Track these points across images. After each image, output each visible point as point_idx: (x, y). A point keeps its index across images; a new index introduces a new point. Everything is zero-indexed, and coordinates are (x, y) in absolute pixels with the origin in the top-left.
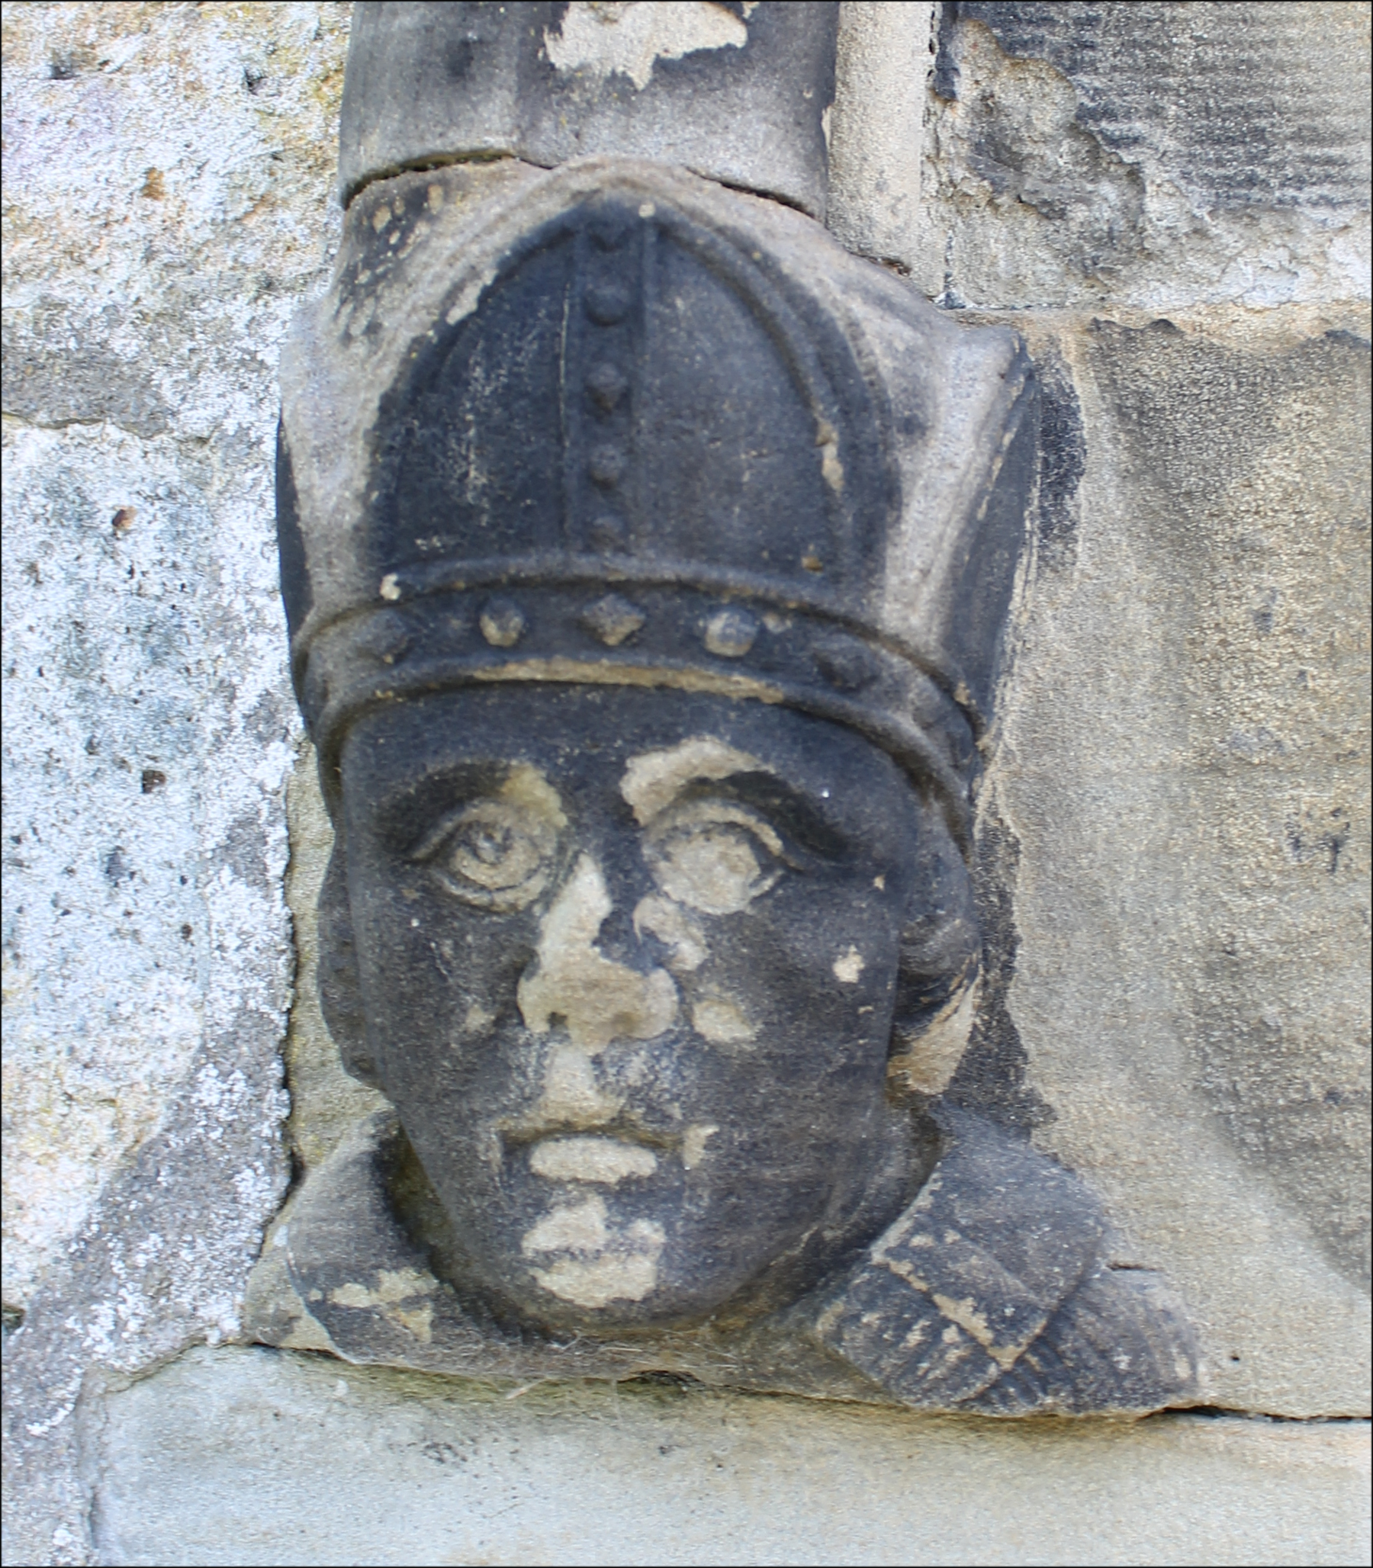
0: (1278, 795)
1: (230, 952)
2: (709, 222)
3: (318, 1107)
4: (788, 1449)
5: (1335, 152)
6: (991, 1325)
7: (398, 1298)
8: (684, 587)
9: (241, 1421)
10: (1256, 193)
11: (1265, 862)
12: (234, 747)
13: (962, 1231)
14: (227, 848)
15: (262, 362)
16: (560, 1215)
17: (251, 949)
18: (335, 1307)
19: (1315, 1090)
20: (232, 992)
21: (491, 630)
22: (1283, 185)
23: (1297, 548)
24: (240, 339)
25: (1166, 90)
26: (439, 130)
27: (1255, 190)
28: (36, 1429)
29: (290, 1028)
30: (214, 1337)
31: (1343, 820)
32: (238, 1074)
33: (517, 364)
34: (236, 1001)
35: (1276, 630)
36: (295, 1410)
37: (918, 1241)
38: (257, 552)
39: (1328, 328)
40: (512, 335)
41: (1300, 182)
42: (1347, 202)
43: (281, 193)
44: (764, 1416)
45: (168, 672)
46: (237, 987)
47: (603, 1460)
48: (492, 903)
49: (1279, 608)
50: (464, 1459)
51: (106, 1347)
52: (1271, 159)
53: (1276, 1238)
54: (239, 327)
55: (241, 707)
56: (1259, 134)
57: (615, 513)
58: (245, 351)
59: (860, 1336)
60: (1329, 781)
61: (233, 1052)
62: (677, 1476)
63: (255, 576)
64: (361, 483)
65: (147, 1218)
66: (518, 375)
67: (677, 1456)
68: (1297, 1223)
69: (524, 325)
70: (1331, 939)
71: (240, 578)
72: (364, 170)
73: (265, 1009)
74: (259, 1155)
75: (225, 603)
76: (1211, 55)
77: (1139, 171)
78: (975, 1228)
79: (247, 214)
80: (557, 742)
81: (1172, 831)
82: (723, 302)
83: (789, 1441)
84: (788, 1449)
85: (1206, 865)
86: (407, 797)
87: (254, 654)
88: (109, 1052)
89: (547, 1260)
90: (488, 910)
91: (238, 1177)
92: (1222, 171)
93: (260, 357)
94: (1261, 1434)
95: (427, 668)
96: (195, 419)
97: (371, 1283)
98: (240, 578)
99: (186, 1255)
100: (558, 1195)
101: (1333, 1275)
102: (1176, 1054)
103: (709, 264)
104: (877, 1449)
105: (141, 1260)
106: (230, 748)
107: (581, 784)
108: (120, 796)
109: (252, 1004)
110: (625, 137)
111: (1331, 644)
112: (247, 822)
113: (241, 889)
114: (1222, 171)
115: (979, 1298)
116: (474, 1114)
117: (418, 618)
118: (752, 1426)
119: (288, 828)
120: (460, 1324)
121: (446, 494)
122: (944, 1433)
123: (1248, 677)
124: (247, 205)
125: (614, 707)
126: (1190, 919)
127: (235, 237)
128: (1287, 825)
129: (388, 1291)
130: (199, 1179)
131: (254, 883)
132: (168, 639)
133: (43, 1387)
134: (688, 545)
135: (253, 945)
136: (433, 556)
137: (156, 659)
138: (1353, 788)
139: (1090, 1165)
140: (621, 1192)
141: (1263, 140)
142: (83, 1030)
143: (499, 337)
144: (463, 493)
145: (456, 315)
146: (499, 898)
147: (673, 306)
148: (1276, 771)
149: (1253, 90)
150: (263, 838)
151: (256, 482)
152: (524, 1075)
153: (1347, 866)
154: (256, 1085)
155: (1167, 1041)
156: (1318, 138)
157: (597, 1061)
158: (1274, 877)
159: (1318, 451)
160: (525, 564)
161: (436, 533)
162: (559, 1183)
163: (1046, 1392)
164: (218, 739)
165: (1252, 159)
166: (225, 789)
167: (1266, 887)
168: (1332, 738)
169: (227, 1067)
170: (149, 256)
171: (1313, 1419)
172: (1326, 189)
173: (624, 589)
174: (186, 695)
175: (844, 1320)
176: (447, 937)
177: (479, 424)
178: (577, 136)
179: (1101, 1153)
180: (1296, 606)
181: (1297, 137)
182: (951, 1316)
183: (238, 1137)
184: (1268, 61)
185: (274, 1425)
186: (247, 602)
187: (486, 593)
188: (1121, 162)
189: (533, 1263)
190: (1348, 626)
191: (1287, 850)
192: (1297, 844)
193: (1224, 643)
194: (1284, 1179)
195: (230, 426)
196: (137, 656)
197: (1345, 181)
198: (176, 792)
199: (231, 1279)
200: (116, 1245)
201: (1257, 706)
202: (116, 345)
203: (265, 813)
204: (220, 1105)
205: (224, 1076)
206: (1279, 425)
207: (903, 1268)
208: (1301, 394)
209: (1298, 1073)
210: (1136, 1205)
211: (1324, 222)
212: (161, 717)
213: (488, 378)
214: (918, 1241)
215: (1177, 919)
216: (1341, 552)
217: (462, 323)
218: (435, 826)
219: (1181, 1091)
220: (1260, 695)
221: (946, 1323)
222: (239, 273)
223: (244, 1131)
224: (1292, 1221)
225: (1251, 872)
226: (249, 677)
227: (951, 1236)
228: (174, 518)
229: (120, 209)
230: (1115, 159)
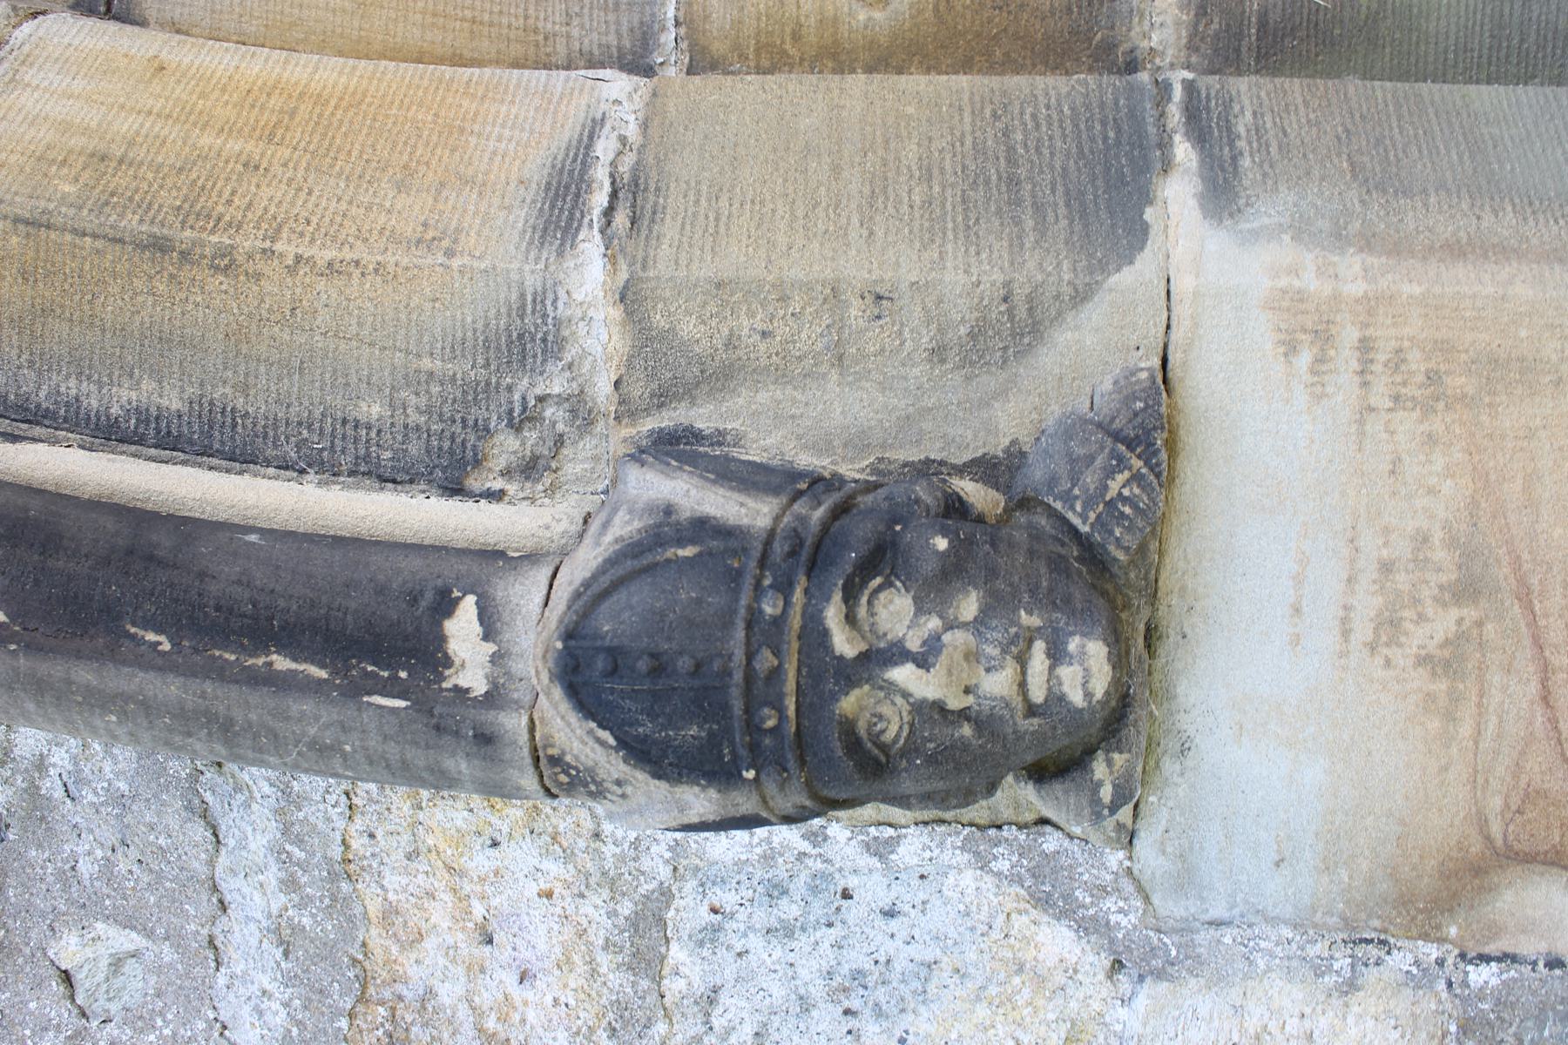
2: (565, 613)
3: (1011, 811)
5: (529, 298)
6: (1121, 472)
8: (749, 626)
9: (1169, 850)
10: (550, 338)
13: (1073, 486)
19: (1003, 308)
25: (498, 383)
28: (1174, 953)
29: (971, 825)
30: (1127, 863)
34: (958, 852)
37: (1078, 509)
41: (545, 316)
45: (792, 886)
49: (760, 326)
51: (1132, 917)
53: (1077, 328)
54: (618, 850)
56: (521, 336)
65: (1068, 897)
67: (1187, 630)
76: (480, 361)
82: (605, 607)
88: (983, 916)
89: (1088, 695)
90: (912, 725)
94: (1175, 335)
96: (664, 872)
97: (1100, 784)
99: (1086, 877)
100: (1056, 689)
102: (984, 378)
105: (1088, 900)
106: (830, 855)
107: (848, 678)
108: (854, 911)
112: (867, 846)
113: (901, 850)
115: (1107, 477)
116: (1015, 732)
123: (794, 342)
124: (556, 847)
126: (916, 371)
130: (1047, 870)
132: (775, 886)
133: (1152, 949)
137: (785, 892)
142: (972, 929)
145: (612, 741)
146: (906, 719)
150: (876, 838)
151: (696, 842)
157: (988, 670)
160: (737, 706)
162: (1049, 689)
167: (900, 333)
170: (582, 896)
172: (548, 303)
173: (750, 656)
174: (804, 877)
181: (522, 318)
187: (752, 726)
192: (879, 317)
194: (1047, 323)
195: (668, 855)
196: (784, 902)
198: (852, 882)
200: (1080, 913)
202: (627, 912)
205: (995, 858)
207: (1092, 516)
212: (814, 890)
214: (1078, 509)
217: (616, 738)
218: (869, 752)
220: (804, 336)
221: (1120, 494)
227: (1076, 491)
228: (714, 883)
229: (558, 910)
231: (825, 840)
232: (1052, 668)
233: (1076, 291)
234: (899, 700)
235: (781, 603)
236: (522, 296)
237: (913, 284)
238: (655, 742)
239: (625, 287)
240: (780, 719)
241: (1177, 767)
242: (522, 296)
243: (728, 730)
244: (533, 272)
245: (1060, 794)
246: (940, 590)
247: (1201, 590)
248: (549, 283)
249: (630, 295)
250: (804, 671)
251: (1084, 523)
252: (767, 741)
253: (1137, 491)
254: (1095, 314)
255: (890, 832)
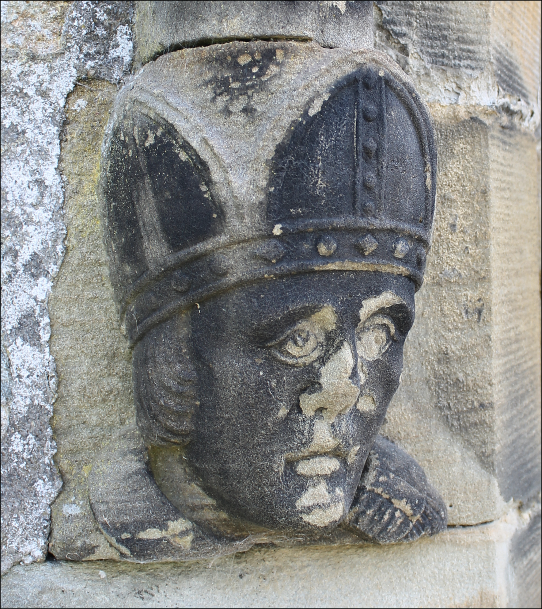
0: (460, 294)
1: (24, 378)
2: (401, 80)
3: (69, 447)
4: (291, 567)
5: (471, 48)
6: (412, 508)
7: (178, 532)
8: (391, 231)
10: (446, 61)
11: (456, 319)
12: (19, 280)
13: (394, 472)
14: (19, 328)
15: (26, 93)
16: (311, 490)
17: (35, 376)
18: (140, 540)
19: (476, 404)
20: (26, 397)
21: (323, 249)
22: (454, 59)
23: (463, 200)
24: (15, 81)
25: (412, 15)
26: (282, 24)
27: (445, 59)
29: (55, 411)
31: (482, 302)
32: (30, 436)
33: (338, 136)
34: (28, 401)
35: (457, 231)
36: (70, 587)
37: (381, 479)
38: (25, 185)
39: (470, 115)
40: (336, 123)
41: (460, 59)
42: (477, 68)
43: (31, 11)
44: (280, 556)
46: (28, 394)
47: (215, 586)
48: (297, 363)
50: (153, 596)
52: (450, 48)
53: (464, 460)
55: (21, 261)
56: (445, 37)
57: (373, 201)
58: (17, 88)
59: (365, 520)
60: (476, 288)
61: (28, 425)
62: (246, 586)
63: (25, 197)
64: (264, 183)
66: (339, 141)
67: (245, 579)
68: (471, 453)
69: (341, 119)
70: (479, 347)
71: (17, 198)
72: (233, 33)
73: (42, 404)
74: (45, 472)
75: (10, 209)
77: (406, 47)
78: (397, 471)
79: (15, 20)
80: (338, 295)
81: (424, 309)
82: (404, 113)
83: (291, 564)
84: (291, 567)
85: (436, 321)
86: (277, 321)
87: (28, 235)
89: (309, 510)
90: (293, 366)
91: (36, 484)
92: (433, 51)
93: (25, 91)
95: (294, 265)
97: (163, 526)
98: (17, 198)
99: (15, 524)
100: (310, 482)
101: (483, 471)
102: (428, 394)
103: (399, 96)
104: (326, 561)
106: (17, 280)
109: (36, 402)
110: (339, 34)
111: (476, 237)
112: (29, 315)
113: (27, 348)
114: (433, 51)
115: (407, 498)
117: (288, 243)
118: (276, 560)
119: (50, 318)
120: (204, 539)
121: (307, 190)
122: (350, 551)
123: (448, 249)
124: (15, 16)
125: (359, 280)
126: (431, 342)
127: (10, 30)
128: (464, 305)
129: (173, 530)
130: (17, 487)
131: (35, 345)
134: (395, 214)
135: (36, 374)
136: (298, 216)
138: (484, 290)
139: (399, 439)
140: (332, 477)
141: (446, 40)
143: (331, 124)
144: (314, 190)
145: (312, 112)
146: (300, 361)
147: (390, 114)
148: (459, 284)
149: (442, 19)
150: (38, 323)
151: (23, 152)
152: (303, 434)
153: (483, 320)
154: (40, 440)
155: (425, 389)
156: (464, 42)
157: (333, 425)
158: (460, 325)
159: (469, 163)
160: (339, 222)
161: (301, 207)
162: (311, 477)
163: (423, 530)
164: (10, 276)
165: (443, 47)
166: (15, 301)
167: (456, 328)
168: (477, 272)
169: (25, 432)
171: (477, 525)
172: (469, 62)
173: (372, 232)
175: (358, 514)
176: (275, 378)
177: (323, 161)
178: (322, 32)
179: (403, 434)
180: (464, 222)
181: (457, 40)
182: (397, 506)
183: (34, 465)
184: (447, 9)
185: (61, 596)
186: (22, 209)
187: (320, 235)
188: (399, 43)
189: (301, 512)
190: (481, 230)
191: (463, 314)
192: (467, 312)
193: (440, 236)
194: (466, 437)
197: (475, 59)
199: (36, 532)
201: (452, 260)
203: (38, 312)
204: (24, 451)
205: (24, 437)
206: (455, 152)
207: (379, 490)
208: (463, 141)
209: (470, 398)
210: (416, 453)
211: (471, 75)
213: (327, 141)
214: (381, 479)
215: (427, 342)
216: (477, 202)
217: (315, 116)
219: (430, 407)
220: (453, 256)
221: (396, 509)
222: (16, 49)
223: (36, 462)
224: (469, 453)
225: (452, 324)
226: (25, 246)
227: (392, 475)
230: (396, 41)
231: (33, 275)
232: (325, 477)
233: (488, 457)
234: (316, 355)
235: (401, 257)
236: (472, 42)
237: (489, 336)
238: (311, 149)
239: (481, 122)
240: (324, 257)
241: (124, 590)
242: (472, 42)
243: (319, 213)
244: (488, 52)
245: (143, 493)
246: (381, 379)
247: (279, 584)
248: (481, 64)
249: (476, 125)
250: (352, 276)
251: (372, 485)
252: (306, 246)
253: (398, 523)
254: (474, 471)
255: (45, 337)
